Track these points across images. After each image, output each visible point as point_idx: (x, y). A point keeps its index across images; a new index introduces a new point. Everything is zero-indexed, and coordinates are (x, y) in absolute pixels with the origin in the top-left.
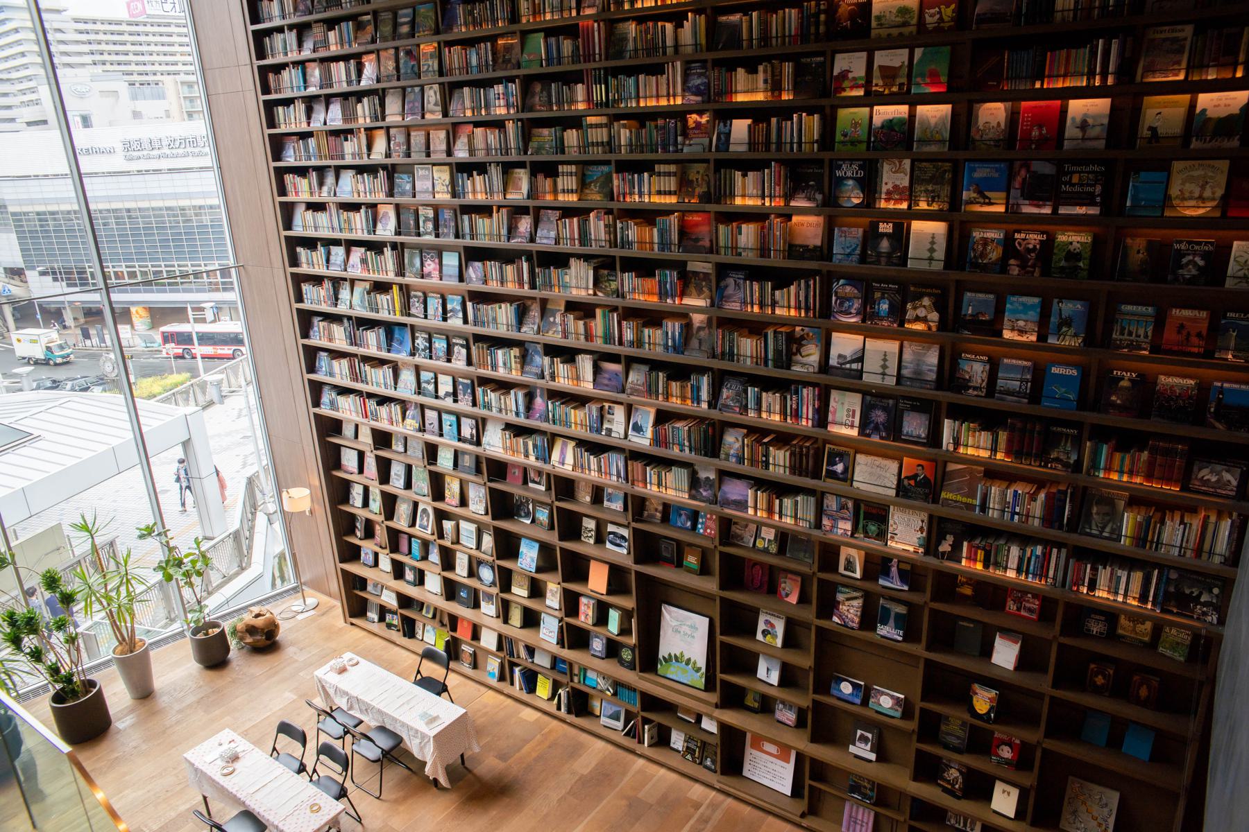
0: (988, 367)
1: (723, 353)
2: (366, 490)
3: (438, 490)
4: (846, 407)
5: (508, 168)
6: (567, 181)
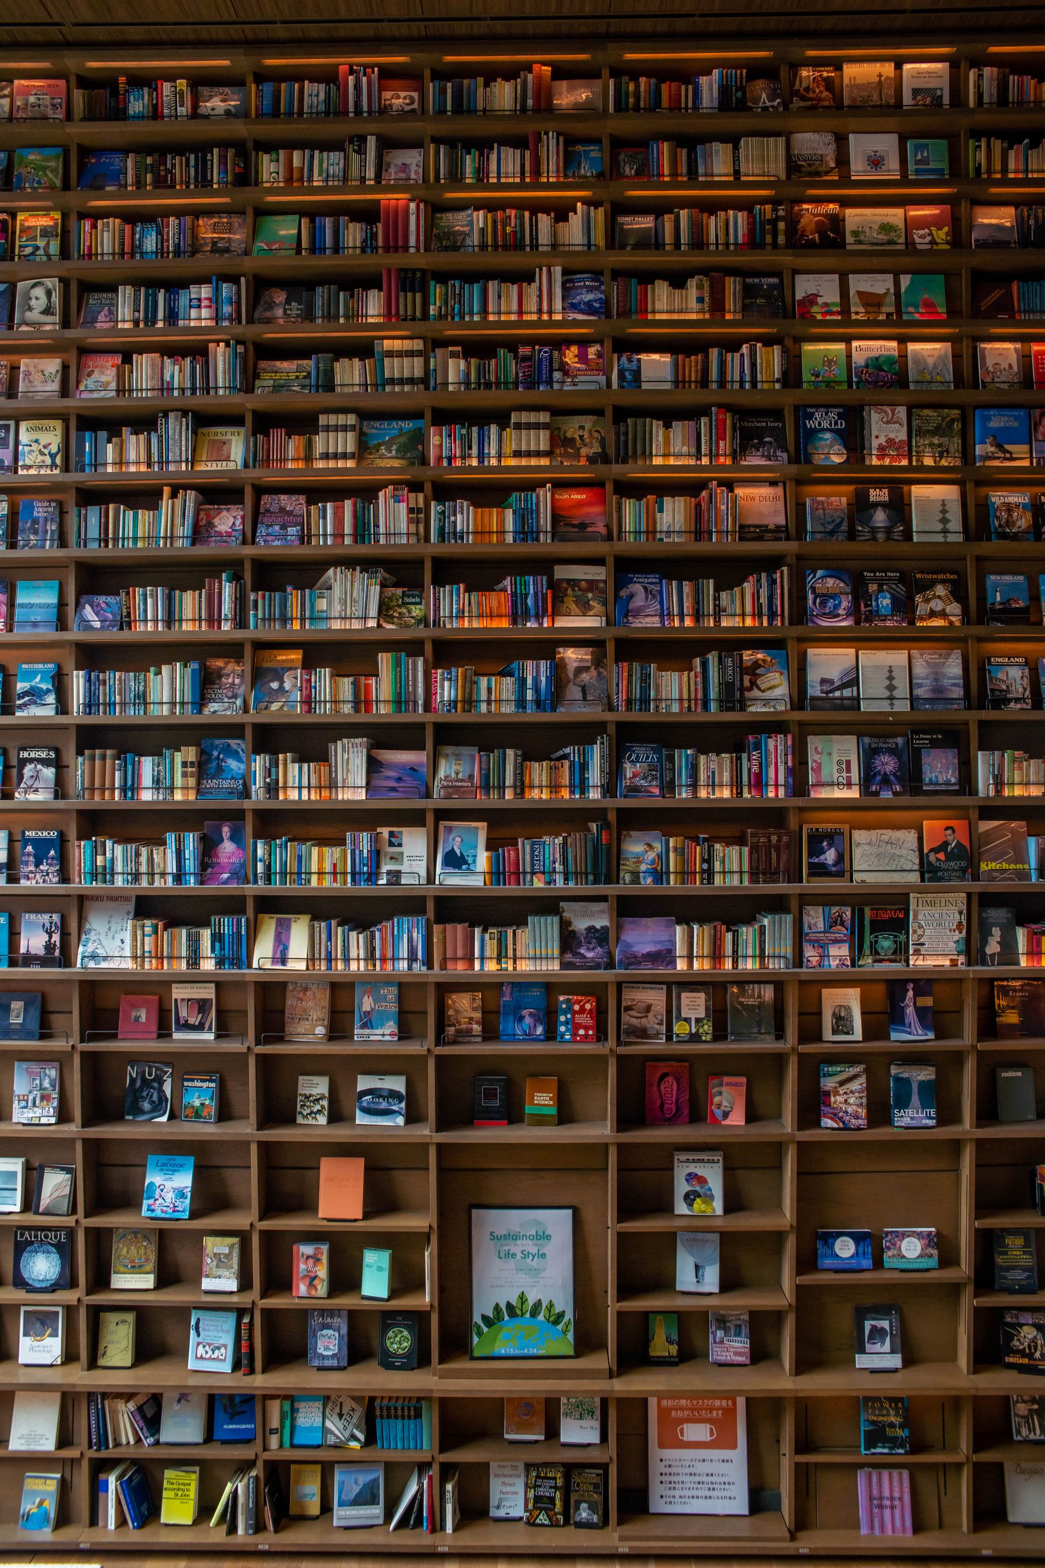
0: (1027, 671)
4: (835, 758)
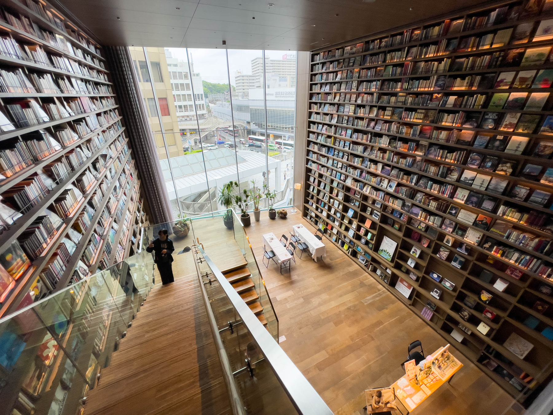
0: (528, 191)
1: (424, 170)
2: (314, 187)
3: (331, 191)
5: (371, 107)
6: (388, 113)
